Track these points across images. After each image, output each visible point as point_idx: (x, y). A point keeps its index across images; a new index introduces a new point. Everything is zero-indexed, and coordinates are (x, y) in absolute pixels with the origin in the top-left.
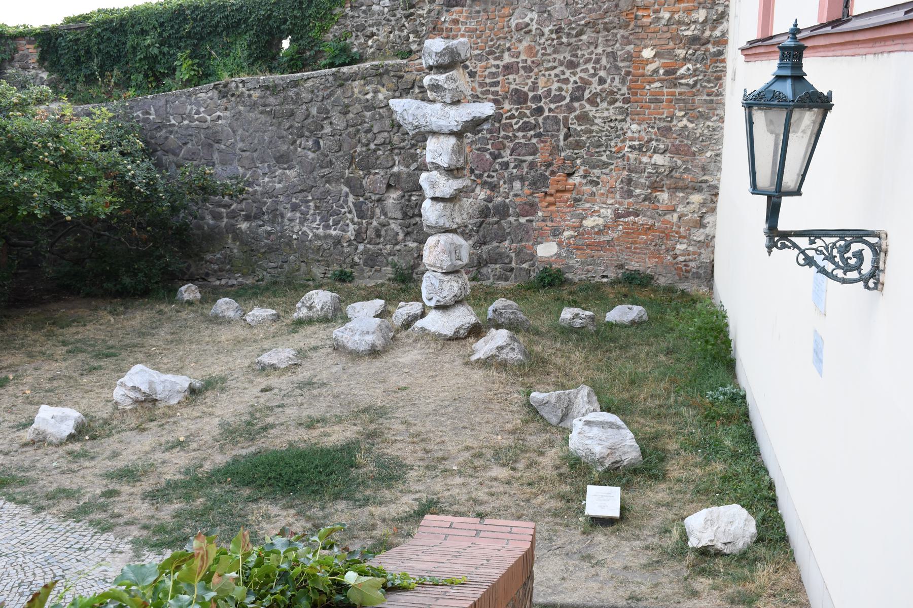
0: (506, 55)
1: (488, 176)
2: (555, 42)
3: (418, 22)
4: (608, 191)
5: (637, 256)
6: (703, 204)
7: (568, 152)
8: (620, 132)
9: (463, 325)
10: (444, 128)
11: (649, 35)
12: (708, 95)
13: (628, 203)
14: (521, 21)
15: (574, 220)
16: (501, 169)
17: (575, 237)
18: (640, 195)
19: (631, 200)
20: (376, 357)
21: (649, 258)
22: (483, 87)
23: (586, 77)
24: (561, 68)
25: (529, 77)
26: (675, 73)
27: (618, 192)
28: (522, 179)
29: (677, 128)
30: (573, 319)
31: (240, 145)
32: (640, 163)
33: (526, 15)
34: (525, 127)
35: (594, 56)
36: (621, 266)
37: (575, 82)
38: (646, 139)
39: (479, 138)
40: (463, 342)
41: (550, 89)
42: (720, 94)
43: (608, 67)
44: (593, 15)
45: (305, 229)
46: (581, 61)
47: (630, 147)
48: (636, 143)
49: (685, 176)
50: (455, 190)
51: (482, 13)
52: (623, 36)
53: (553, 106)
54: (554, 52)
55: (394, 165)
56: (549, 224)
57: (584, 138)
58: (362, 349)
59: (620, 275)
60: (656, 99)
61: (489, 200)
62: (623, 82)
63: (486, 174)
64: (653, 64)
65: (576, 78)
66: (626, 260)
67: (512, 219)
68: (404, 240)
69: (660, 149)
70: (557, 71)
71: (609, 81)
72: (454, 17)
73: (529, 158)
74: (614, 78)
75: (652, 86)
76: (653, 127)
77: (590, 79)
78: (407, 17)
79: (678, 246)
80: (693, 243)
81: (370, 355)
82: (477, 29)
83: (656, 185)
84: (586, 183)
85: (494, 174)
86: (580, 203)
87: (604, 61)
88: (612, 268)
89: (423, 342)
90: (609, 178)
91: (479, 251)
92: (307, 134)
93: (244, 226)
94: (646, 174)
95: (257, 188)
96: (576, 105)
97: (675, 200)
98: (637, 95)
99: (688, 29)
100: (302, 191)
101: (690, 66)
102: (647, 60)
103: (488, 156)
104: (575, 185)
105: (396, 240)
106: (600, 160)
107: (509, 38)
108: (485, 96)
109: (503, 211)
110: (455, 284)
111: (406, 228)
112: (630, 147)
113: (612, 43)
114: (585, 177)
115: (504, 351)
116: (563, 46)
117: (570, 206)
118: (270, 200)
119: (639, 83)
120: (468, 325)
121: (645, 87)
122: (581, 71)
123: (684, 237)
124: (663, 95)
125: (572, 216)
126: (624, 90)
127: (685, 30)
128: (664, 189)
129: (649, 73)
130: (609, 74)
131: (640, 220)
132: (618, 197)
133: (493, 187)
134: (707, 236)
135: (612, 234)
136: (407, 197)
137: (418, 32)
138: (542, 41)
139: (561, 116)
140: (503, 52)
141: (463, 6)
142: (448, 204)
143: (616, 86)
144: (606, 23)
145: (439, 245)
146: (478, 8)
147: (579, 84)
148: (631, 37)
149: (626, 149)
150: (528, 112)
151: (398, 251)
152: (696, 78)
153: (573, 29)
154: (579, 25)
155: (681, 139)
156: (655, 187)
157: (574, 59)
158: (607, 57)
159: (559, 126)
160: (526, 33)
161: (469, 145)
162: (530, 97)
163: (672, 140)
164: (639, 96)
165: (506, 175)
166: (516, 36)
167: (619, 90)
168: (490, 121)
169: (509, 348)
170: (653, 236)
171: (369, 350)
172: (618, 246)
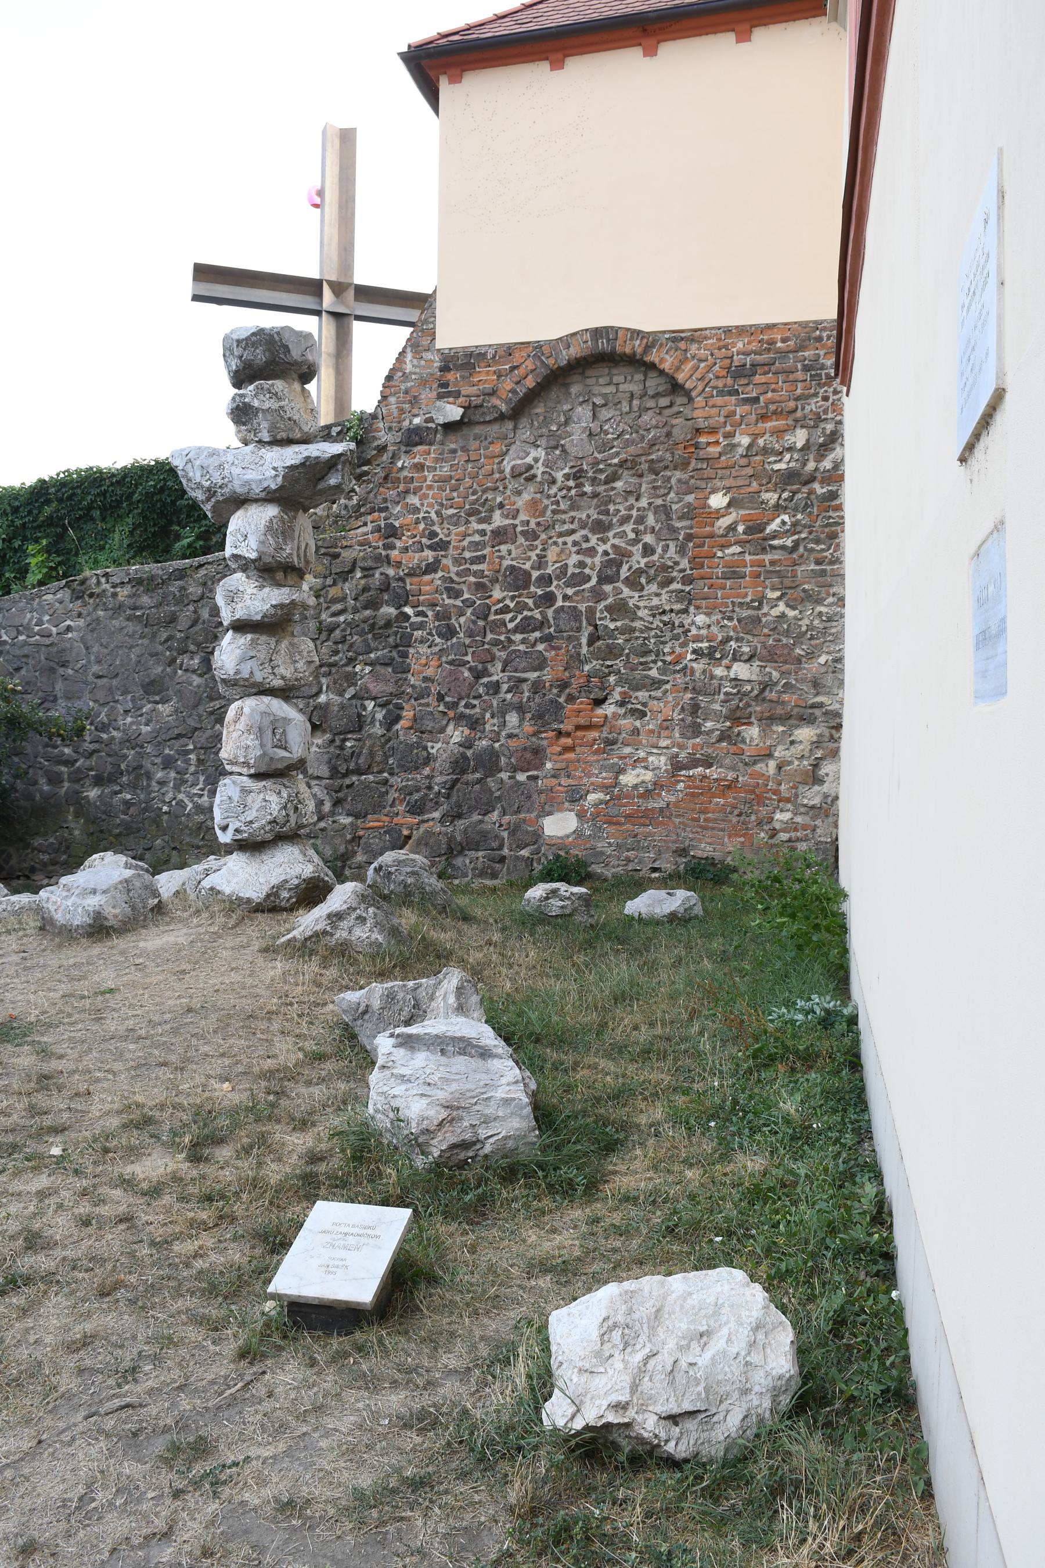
0: (497, 514)
1: (466, 706)
2: (573, 492)
4: (661, 727)
6: (817, 744)
9: (286, 881)
11: (719, 471)
12: (818, 562)
13: (694, 746)
14: (519, 462)
16: (487, 694)
17: (607, 802)
18: (712, 731)
21: (730, 836)
22: (460, 565)
23: (623, 545)
24: (583, 532)
25: (532, 548)
26: (762, 530)
27: (677, 728)
28: (520, 709)
30: (547, 898)
31: (95, 668)
33: (528, 454)
34: (525, 627)
35: (634, 513)
36: (683, 852)
38: (720, 638)
41: (566, 564)
42: (837, 561)
43: (657, 528)
44: (632, 449)
45: (181, 796)
47: (694, 652)
49: (786, 697)
50: (274, 606)
51: (459, 453)
52: (679, 481)
53: (570, 591)
54: (572, 508)
56: (565, 781)
57: (620, 641)
58: (76, 923)
60: (734, 572)
61: (467, 744)
62: (682, 551)
63: (463, 703)
65: (607, 547)
67: (504, 776)
68: (332, 813)
69: (743, 654)
70: (576, 537)
71: (659, 550)
72: (416, 460)
73: (533, 675)
74: (668, 546)
75: (727, 551)
76: (730, 619)
77: (629, 548)
79: (778, 816)
80: (802, 810)
82: (451, 477)
83: (738, 714)
85: (475, 702)
86: (615, 747)
87: (651, 520)
88: (668, 855)
90: (662, 705)
92: (192, 648)
93: (93, 793)
95: (115, 733)
96: (608, 588)
97: (771, 738)
98: (702, 567)
99: (780, 460)
100: (179, 736)
101: (786, 518)
102: (718, 511)
103: (466, 674)
104: (606, 717)
106: (647, 677)
107: (501, 488)
109: (489, 763)
110: (273, 798)
111: (336, 792)
112: (694, 652)
114: (622, 704)
115: (344, 924)
116: (585, 498)
117: (598, 752)
118: (132, 752)
119: (706, 548)
121: (715, 554)
123: (788, 800)
125: (603, 768)
126: (684, 563)
127: (775, 462)
128: (753, 719)
129: (721, 532)
130: (659, 539)
131: (714, 773)
132: (677, 735)
133: (475, 724)
134: (826, 796)
135: (667, 797)
136: (338, 743)
138: (552, 491)
139: (582, 607)
140: (491, 510)
141: (431, 444)
142: (264, 638)
143: (670, 558)
146: (453, 446)
149: (689, 657)
150: (530, 602)
152: (796, 537)
153: (601, 471)
154: (610, 465)
155: (776, 636)
156: (738, 717)
158: (655, 513)
159: (581, 622)
160: (528, 479)
162: (533, 578)
165: (495, 703)
166: (512, 485)
167: (677, 563)
170: (735, 798)
172: (678, 816)
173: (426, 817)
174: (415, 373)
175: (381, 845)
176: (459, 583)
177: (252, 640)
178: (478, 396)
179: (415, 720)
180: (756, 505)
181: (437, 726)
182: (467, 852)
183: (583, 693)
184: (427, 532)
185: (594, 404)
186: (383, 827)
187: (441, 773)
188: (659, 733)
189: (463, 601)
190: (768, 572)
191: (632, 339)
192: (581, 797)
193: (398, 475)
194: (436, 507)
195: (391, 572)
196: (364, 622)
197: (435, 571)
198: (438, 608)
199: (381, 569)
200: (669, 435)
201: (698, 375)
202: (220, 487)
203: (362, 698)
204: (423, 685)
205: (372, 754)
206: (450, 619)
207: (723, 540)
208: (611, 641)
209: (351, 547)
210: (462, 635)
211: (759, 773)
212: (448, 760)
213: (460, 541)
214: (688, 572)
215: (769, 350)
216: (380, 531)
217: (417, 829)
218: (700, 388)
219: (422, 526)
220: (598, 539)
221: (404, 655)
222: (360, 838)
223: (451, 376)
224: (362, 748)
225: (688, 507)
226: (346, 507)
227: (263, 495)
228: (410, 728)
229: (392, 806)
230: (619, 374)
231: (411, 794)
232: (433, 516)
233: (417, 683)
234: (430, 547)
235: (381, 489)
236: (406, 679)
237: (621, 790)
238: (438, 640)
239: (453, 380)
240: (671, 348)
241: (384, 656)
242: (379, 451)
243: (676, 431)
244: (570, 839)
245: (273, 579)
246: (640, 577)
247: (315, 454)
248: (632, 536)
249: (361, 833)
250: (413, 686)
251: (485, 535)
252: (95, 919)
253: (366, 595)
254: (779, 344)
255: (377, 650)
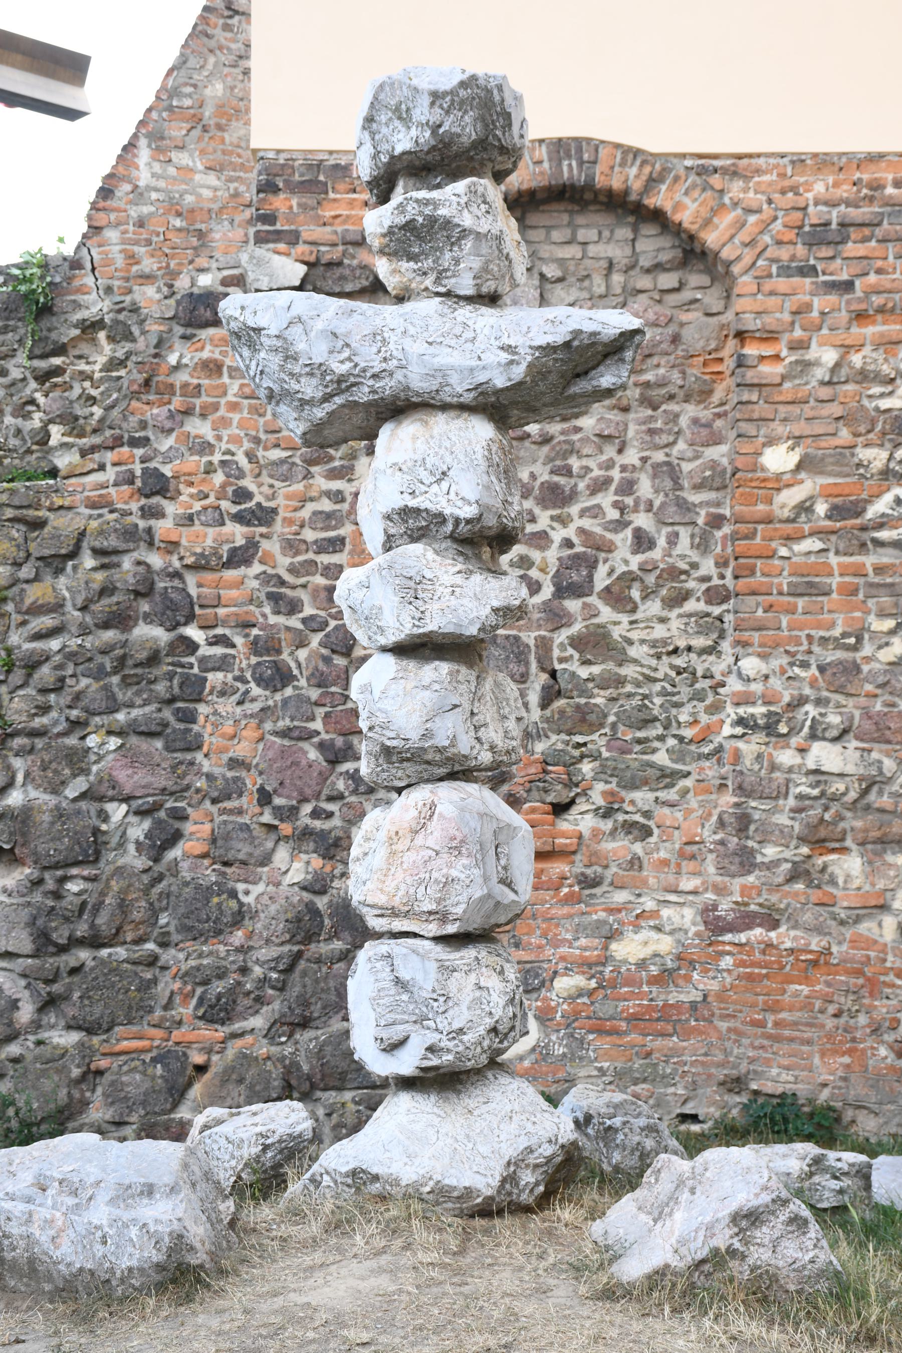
1: (316, 814)
3: (77, 391)
4: (681, 854)
5: (785, 1048)
7: (556, 741)
8: (701, 684)
9: (530, 1150)
10: (454, 379)
11: (782, 409)
13: (744, 890)
15: (583, 941)
16: (355, 792)
17: (591, 993)
18: (776, 863)
19: (751, 879)
20: (189, 1299)
21: (823, 1054)
22: (297, 553)
23: (598, 530)
26: (860, 513)
27: (711, 857)
29: (876, 666)
30: (811, 1175)
32: (773, 767)
36: (735, 1084)
37: (568, 543)
38: (786, 699)
39: (285, 702)
40: (536, 1222)
43: (657, 503)
46: (581, 486)
47: (740, 721)
48: (759, 710)
50: (496, 610)
52: (695, 421)
55: (10, 784)
57: (599, 701)
58: (125, 1263)
59: (735, 1112)
60: (810, 584)
62: (703, 544)
63: (307, 808)
64: (795, 489)
65: (570, 532)
66: (752, 1061)
68: (36, 1025)
69: (829, 727)
71: (662, 542)
72: (205, 354)
74: (677, 535)
75: (796, 548)
76: (805, 665)
77: (609, 536)
78: (43, 377)
81: (161, 1288)
83: (822, 833)
84: (615, 830)
86: (597, 891)
87: (645, 487)
88: (710, 1091)
89: (372, 1228)
90: (679, 815)
91: (289, 1050)
94: (791, 802)
96: (573, 605)
97: (885, 876)
98: (753, 573)
99: (891, 393)
102: (778, 477)
103: (313, 754)
104: (580, 837)
105: (10, 1024)
106: (651, 765)
108: (303, 580)
110: (492, 981)
111: (48, 982)
112: (740, 721)
113: (665, 439)
114: (607, 813)
115: (763, 1234)
116: (527, 443)
117: (570, 899)
119: (758, 540)
120: (548, 1150)
121: (775, 552)
122: (583, 513)
124: (831, 574)
125: (578, 930)
126: (708, 566)
127: (882, 395)
128: (849, 843)
129: (786, 513)
132: (712, 870)
136: (50, 885)
137: (76, 418)
139: (529, 638)
143: (683, 557)
144: (647, 385)
145: (434, 825)
147: (579, 549)
148: (719, 423)
149: (727, 730)
151: (16, 1060)
155: (888, 698)
157: (561, 480)
158: (655, 476)
159: (527, 664)
161: (254, 722)
163: (863, 701)
164: (759, 578)
167: (694, 566)
168: (628, 354)
169: (784, 1216)
170: (828, 984)
171: (160, 1267)
173: (237, 1026)
174: (157, 190)
175: (147, 1085)
176: (294, 588)
177: (450, 673)
178: (335, 245)
179: (214, 841)
180: (846, 469)
181: (257, 852)
182: (319, 1094)
183: (535, 794)
184: (230, 490)
185: (542, 276)
186: (149, 1050)
187: (268, 941)
188: (679, 865)
189: (304, 621)
190: (871, 585)
191: (623, 164)
192: (543, 984)
193: (170, 380)
194: (247, 445)
195: (156, 560)
196: (103, 652)
197: (247, 562)
198: (255, 632)
199: (135, 555)
200: (676, 339)
201: (744, 236)
202: (375, 376)
203: (101, 799)
204: (230, 774)
205: (123, 906)
206: (279, 652)
207: (789, 528)
208: (583, 701)
209: (69, 508)
210: (303, 682)
211: (868, 939)
212: (283, 917)
213: (296, 510)
214: (716, 581)
215: (871, 199)
216: (131, 482)
217: (221, 1052)
218: (747, 260)
219: (219, 478)
220: (552, 518)
221: (189, 717)
222: (100, 1073)
223: (282, 203)
224: (103, 894)
225: (712, 468)
226: (19, 432)
227: (468, 398)
228: (204, 856)
229: (167, 1007)
230: (587, 226)
231: (206, 982)
232: (243, 461)
233: (217, 771)
234: (239, 518)
235: (135, 404)
236: (192, 763)
237: (616, 970)
238: (256, 690)
239: (284, 210)
240: (694, 186)
241: (148, 719)
242: (83, 331)
243: (687, 334)
244: (527, 1063)
245: (478, 557)
246: (629, 588)
247: (588, 327)
248: (614, 514)
249: (103, 1063)
250: (210, 777)
251: (343, 500)
252: (171, 1251)
253: (105, 601)
254: (890, 190)
255: (131, 705)
